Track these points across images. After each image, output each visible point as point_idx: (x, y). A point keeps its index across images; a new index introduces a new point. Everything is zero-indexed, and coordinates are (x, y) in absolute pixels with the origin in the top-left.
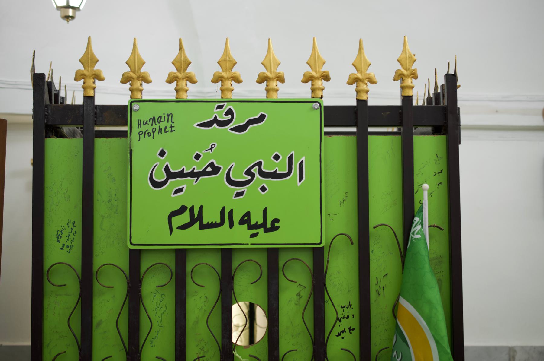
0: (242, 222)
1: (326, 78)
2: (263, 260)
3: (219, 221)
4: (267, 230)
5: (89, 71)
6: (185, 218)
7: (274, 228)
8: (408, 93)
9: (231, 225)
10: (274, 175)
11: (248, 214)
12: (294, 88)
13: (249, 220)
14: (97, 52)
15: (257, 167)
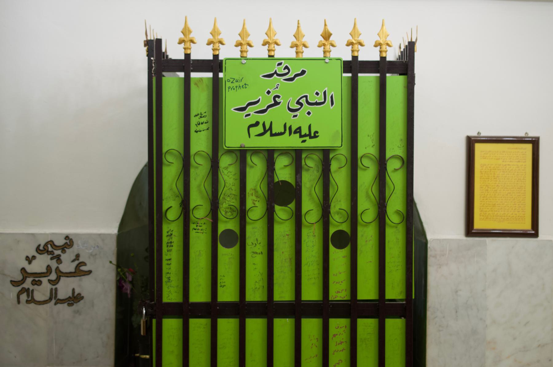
0: (295, 132)
1: (221, 43)
2: (321, 155)
3: (283, 131)
4: (311, 137)
5: (186, 40)
6: (260, 129)
7: (315, 137)
8: (356, 54)
9: (290, 134)
10: (317, 104)
11: (300, 128)
12: (258, 51)
13: (300, 132)
14: (191, 26)
15: (305, 98)
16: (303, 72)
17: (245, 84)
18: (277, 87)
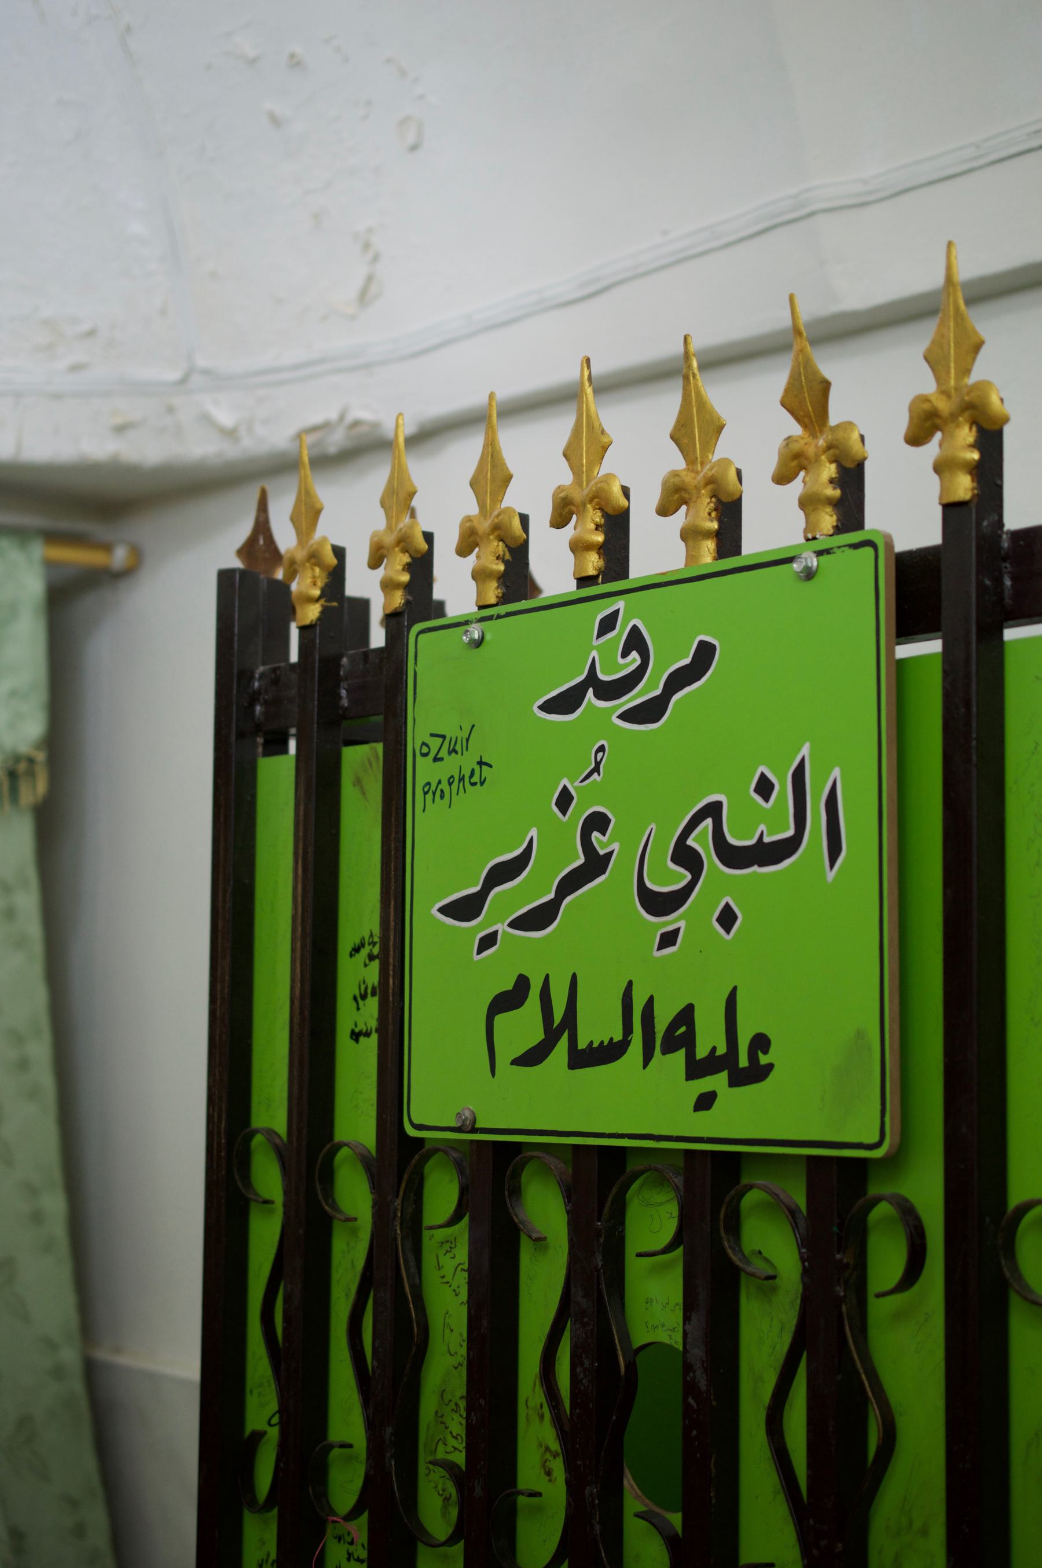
0: (669, 1047)
4: (739, 1078)
7: (758, 1073)
11: (686, 1015)
13: (688, 1042)
16: (705, 654)
17: (481, 763)
18: (596, 769)
